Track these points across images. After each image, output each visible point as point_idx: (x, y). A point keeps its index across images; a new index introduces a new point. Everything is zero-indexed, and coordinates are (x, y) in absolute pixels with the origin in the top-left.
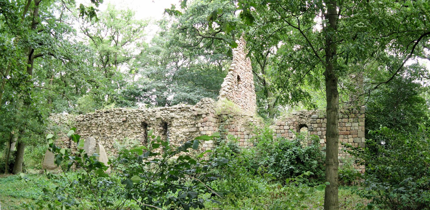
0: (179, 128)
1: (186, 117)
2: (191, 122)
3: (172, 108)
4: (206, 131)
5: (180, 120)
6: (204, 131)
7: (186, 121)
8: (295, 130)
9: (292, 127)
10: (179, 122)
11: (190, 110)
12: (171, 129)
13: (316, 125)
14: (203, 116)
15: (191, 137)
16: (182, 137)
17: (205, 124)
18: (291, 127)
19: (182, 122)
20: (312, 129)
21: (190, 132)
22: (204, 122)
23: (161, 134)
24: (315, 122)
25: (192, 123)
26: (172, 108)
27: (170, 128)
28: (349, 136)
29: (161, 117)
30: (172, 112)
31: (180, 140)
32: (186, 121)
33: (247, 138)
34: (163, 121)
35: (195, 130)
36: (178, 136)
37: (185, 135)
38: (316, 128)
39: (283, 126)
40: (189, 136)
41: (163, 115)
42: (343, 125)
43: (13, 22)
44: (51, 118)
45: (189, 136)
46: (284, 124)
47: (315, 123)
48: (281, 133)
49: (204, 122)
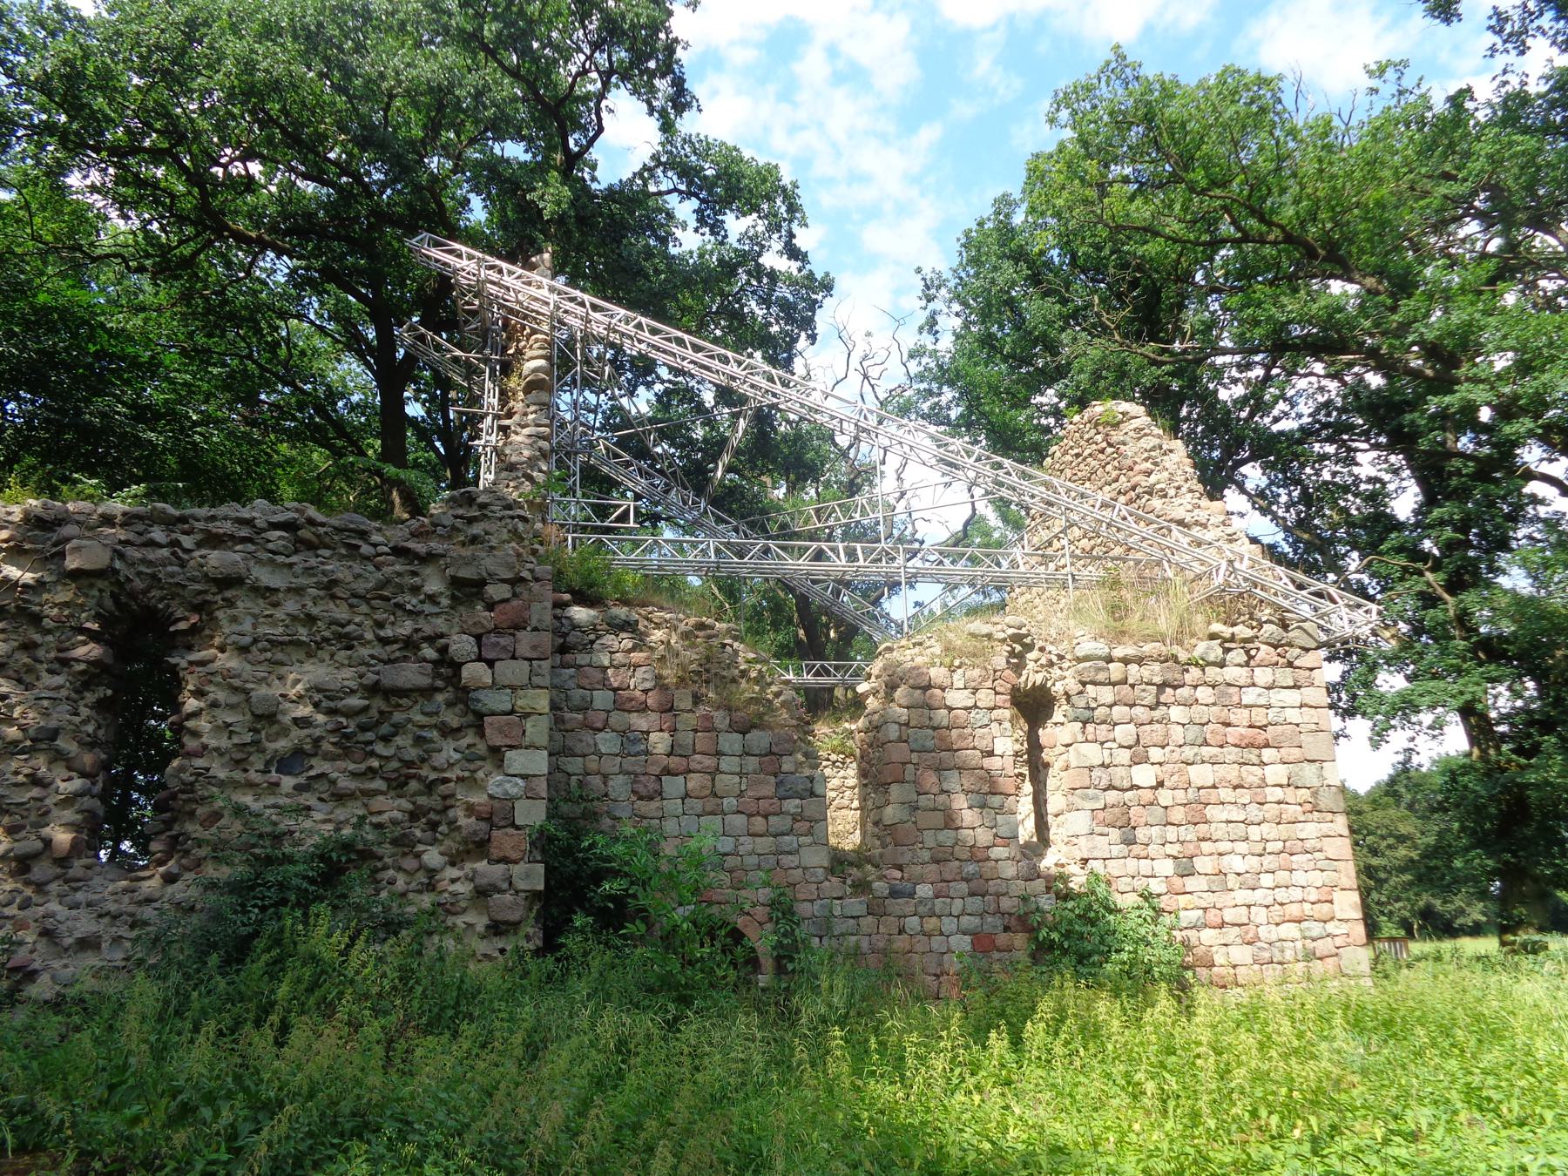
0: (280, 656)
1: (338, 591)
2: (380, 625)
3: (213, 518)
4: (514, 688)
5: (291, 606)
6: (495, 686)
7: (341, 612)
8: (1007, 714)
9: (985, 698)
10: (279, 614)
11: (366, 549)
12: (202, 663)
13: (1107, 695)
14: (495, 591)
15: (385, 729)
16: (302, 723)
17: (503, 641)
18: (981, 694)
19: (311, 619)
20: (1087, 713)
21: (374, 690)
22: (496, 630)
23: (90, 697)
24: (1101, 677)
25: (388, 632)
26: (213, 518)
27: (196, 656)
28: (1268, 754)
29: (118, 564)
30: (213, 540)
31: (282, 745)
32: (341, 612)
33: (738, 748)
34: (133, 595)
35: (424, 681)
36: (270, 718)
37: (331, 712)
38: (1111, 706)
39: (943, 690)
40: (363, 719)
41: (133, 553)
42: (1230, 696)
43: (150, 52)
44: (1503, 581)
45: (363, 719)
46: (947, 682)
47: (1101, 684)
48: (934, 728)
49: (496, 630)
